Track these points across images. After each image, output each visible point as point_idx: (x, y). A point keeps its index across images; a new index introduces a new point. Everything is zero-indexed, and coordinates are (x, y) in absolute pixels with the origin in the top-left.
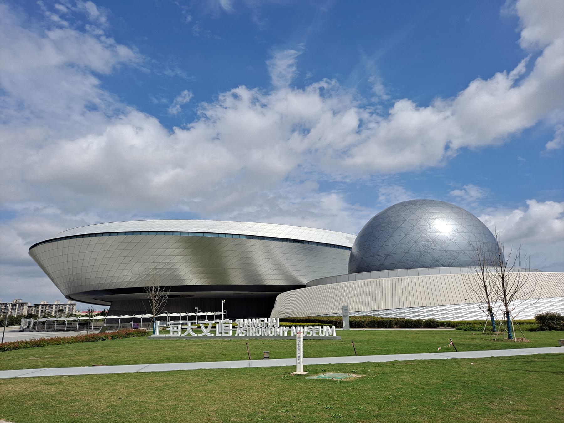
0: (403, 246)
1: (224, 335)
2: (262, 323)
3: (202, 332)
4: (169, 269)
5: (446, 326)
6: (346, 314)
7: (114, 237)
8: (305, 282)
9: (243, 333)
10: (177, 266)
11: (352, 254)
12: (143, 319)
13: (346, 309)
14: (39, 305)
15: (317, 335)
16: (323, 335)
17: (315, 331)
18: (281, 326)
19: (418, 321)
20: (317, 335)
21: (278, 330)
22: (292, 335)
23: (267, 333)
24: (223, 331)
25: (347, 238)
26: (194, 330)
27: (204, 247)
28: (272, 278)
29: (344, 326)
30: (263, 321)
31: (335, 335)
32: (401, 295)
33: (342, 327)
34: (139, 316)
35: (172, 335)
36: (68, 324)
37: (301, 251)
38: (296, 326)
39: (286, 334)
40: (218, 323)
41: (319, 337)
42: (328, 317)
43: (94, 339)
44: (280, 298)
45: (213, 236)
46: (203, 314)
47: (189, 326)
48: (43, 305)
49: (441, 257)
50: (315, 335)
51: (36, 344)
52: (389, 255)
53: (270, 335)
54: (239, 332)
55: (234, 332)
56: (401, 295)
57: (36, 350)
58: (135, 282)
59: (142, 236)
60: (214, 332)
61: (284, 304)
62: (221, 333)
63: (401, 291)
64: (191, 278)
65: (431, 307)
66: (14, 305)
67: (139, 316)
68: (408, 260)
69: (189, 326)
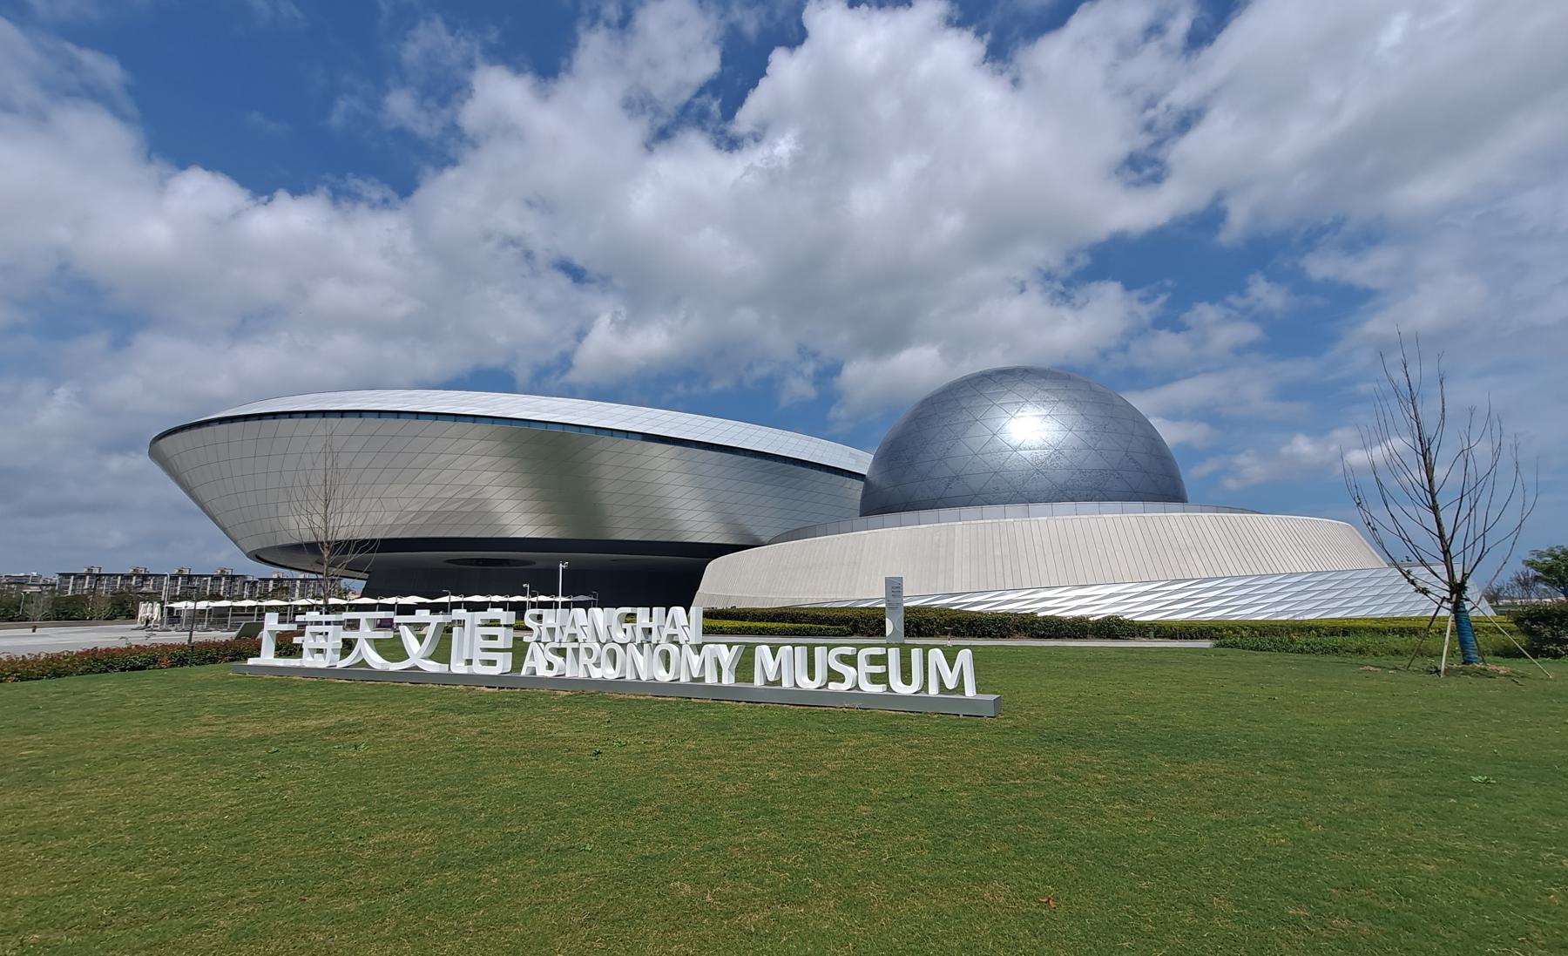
0: (987, 457)
2: (628, 626)
3: (404, 656)
4: (469, 501)
8: (764, 539)
9: (550, 666)
10: (487, 495)
12: (235, 609)
13: (894, 586)
15: (879, 689)
17: (865, 668)
19: (1081, 619)
20: (879, 689)
21: (696, 660)
22: (758, 682)
23: (647, 668)
24: (478, 656)
26: (379, 646)
27: (551, 454)
28: (698, 526)
29: (889, 630)
30: (631, 618)
31: (970, 692)
32: (998, 562)
35: (308, 661)
39: (728, 680)
40: (461, 623)
44: (715, 570)
45: (568, 431)
47: (365, 632)
50: (868, 688)
51: (99, 663)
52: (957, 477)
53: (663, 676)
54: (539, 663)
56: (998, 562)
57: (51, 686)
59: (402, 421)
60: (442, 652)
61: (722, 582)
62: (469, 662)
63: (998, 553)
64: (517, 518)
66: (216, 578)
69: (365, 632)
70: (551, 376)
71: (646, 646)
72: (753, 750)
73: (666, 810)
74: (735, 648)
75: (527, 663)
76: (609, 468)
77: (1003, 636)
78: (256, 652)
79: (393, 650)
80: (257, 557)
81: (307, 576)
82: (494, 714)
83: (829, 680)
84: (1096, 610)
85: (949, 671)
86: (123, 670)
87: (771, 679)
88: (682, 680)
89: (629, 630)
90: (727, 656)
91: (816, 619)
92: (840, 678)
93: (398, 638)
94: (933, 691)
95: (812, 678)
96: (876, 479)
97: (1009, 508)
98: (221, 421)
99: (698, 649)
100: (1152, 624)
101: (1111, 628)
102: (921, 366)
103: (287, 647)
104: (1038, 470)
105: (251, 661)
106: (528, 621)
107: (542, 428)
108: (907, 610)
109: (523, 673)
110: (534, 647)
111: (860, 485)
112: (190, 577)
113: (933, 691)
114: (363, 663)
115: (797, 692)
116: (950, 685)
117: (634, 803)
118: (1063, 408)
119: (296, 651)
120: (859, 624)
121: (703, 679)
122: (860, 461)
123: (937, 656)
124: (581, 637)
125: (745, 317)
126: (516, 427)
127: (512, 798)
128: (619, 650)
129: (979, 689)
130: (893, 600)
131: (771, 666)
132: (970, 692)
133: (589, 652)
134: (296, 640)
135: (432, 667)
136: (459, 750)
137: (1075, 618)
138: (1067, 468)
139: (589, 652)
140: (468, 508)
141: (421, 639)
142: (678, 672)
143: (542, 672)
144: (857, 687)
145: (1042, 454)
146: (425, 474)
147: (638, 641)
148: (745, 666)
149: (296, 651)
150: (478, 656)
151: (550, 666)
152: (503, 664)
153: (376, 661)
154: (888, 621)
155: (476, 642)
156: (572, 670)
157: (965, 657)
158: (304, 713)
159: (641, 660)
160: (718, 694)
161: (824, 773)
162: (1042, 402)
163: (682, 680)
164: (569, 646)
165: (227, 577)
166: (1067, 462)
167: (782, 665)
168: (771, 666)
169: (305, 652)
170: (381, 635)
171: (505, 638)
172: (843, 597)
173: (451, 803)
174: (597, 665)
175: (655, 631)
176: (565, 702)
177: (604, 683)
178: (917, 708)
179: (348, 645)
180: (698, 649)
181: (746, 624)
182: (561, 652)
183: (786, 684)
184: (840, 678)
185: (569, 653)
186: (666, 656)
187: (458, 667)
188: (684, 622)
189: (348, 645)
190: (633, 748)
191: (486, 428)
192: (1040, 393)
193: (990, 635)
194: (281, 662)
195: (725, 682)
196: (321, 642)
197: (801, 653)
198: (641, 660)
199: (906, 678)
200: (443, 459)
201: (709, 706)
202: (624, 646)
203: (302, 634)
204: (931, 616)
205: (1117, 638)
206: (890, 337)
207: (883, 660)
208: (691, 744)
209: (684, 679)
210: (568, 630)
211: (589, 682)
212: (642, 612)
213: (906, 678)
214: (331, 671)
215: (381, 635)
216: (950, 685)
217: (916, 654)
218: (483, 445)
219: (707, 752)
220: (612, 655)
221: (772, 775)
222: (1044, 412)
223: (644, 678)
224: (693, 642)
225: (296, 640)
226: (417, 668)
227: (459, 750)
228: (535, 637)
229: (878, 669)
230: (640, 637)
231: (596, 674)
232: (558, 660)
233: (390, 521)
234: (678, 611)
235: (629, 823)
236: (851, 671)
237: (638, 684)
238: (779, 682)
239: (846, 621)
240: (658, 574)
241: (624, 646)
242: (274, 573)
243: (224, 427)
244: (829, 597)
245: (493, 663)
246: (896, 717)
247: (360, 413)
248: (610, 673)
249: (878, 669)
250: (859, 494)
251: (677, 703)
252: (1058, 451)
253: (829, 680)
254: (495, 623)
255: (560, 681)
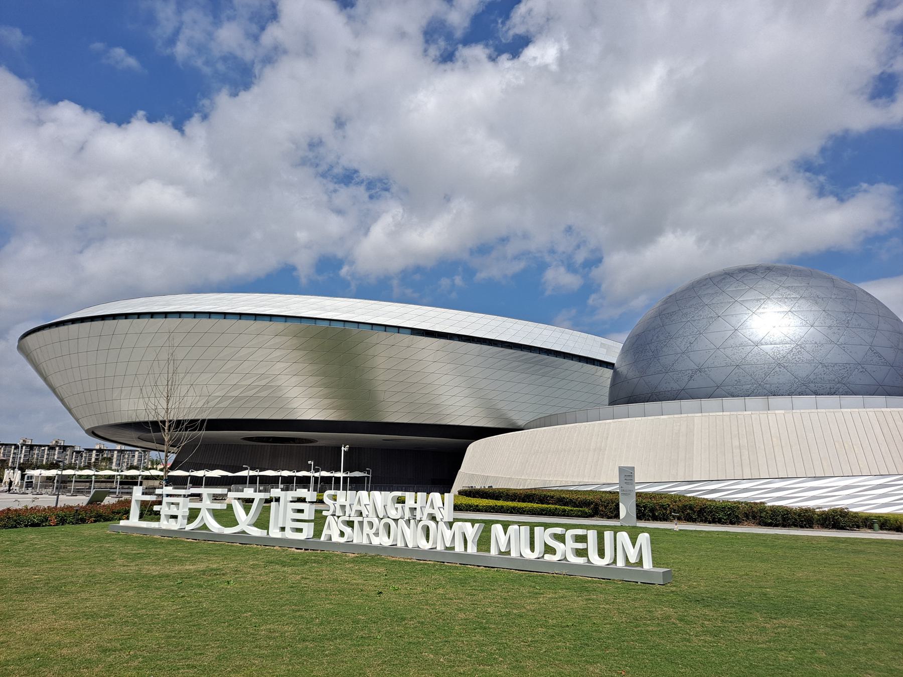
0: (729, 352)
1: (290, 535)
3: (235, 523)
4: (265, 387)
5: (876, 526)
6: (629, 487)
7: (160, 321)
8: (521, 423)
9: (342, 534)
11: (616, 374)
13: (627, 474)
14: (90, 450)
16: (602, 563)
17: (571, 544)
18: (456, 520)
20: (581, 561)
21: (448, 534)
22: (494, 552)
23: (413, 538)
24: (290, 525)
25: (603, 345)
27: (334, 347)
28: (461, 412)
29: (622, 514)
30: (401, 501)
31: (647, 565)
33: (617, 516)
34: (200, 473)
35: (165, 524)
36: (96, 482)
37: (516, 364)
38: (506, 526)
39: (472, 549)
40: (278, 500)
41: (590, 567)
42: (577, 492)
43: (76, 517)
44: (475, 450)
45: (348, 327)
46: (324, 474)
47: (206, 504)
48: (97, 451)
49: (812, 377)
52: (700, 370)
53: (425, 545)
54: (333, 531)
55: (318, 533)
58: (202, 410)
60: (262, 522)
61: (480, 465)
62: (283, 529)
64: (304, 401)
65: (816, 478)
66: (52, 448)
67: (200, 473)
68: (739, 381)
69: (206, 504)
70: (330, 276)
71: (412, 521)
72: (481, 596)
73: (422, 623)
74: (477, 525)
75: (325, 532)
76: (383, 358)
77: (732, 523)
78: (126, 514)
79: (226, 517)
80: (93, 433)
81: (123, 447)
82: (307, 567)
83: (546, 552)
84: (822, 503)
85: (630, 549)
86: (26, 526)
87: (503, 550)
88: (438, 548)
89: (400, 509)
90: (472, 532)
91: (561, 501)
92: (552, 551)
93: (230, 507)
94: (620, 563)
95: (532, 549)
96: (623, 369)
97: (750, 401)
98: (74, 321)
99: (450, 525)
100: (878, 517)
101: (836, 519)
102: (676, 252)
103: (148, 512)
104: (780, 363)
105: (123, 523)
106: (326, 499)
107: (326, 324)
108: (639, 495)
109: (323, 538)
110: (330, 519)
111: (609, 373)
112: (32, 447)
113: (620, 563)
114: (205, 527)
115: (521, 559)
116: (633, 560)
117: (404, 619)
118: (805, 305)
119: (156, 516)
120: (597, 507)
121: (453, 548)
122: (609, 349)
123: (623, 536)
124: (365, 513)
125: (505, 217)
126: (305, 324)
127: (332, 613)
128: (392, 524)
129: (656, 563)
130: (626, 487)
131: (503, 540)
132: (647, 565)
133: (371, 524)
134: (156, 508)
135: (255, 532)
136: (292, 587)
137: (801, 509)
138: (809, 362)
139: (371, 524)
140: (264, 394)
141: (247, 510)
142: (435, 542)
143: (336, 538)
144: (565, 559)
145: (784, 349)
146: (230, 364)
147: (406, 518)
148: (484, 541)
149: (156, 516)
150: (290, 525)
151: (342, 534)
152: (308, 530)
153: (214, 526)
154: (621, 506)
155: (288, 516)
156: (357, 537)
157: (644, 538)
158: (181, 561)
159: (408, 532)
160: (465, 560)
161: (524, 610)
162: (783, 299)
163: (438, 548)
164: (356, 520)
165: (60, 447)
166: (809, 357)
167: (513, 540)
168: (503, 540)
169: (162, 517)
170: (218, 506)
171: (309, 511)
172: (590, 481)
173: (298, 613)
174: (377, 534)
175: (418, 510)
176: (354, 561)
177: (381, 548)
178: (606, 579)
179: (193, 515)
180: (450, 525)
181: (500, 503)
182: (350, 524)
183: (514, 554)
184: (552, 551)
185: (356, 525)
186: (427, 530)
187: (275, 533)
188: (440, 503)
189: (193, 515)
190: (403, 592)
191: (280, 326)
192: (782, 291)
193: (719, 521)
194: (144, 524)
195: (469, 551)
196: (174, 511)
197: (525, 530)
198: (408, 532)
199: (601, 554)
200: (244, 352)
201: (457, 568)
202: (396, 520)
203: (160, 503)
204: (665, 502)
205: (842, 528)
206: (645, 231)
207: (582, 539)
208: (441, 591)
209: (440, 548)
210: (356, 507)
211: (370, 547)
212: (409, 496)
213: (601, 554)
214: (181, 532)
215: (218, 506)
216: (633, 560)
217: (608, 535)
218: (278, 340)
219: (451, 595)
220: (388, 528)
221: (489, 610)
222: (786, 308)
223: (410, 546)
224: (446, 520)
225: (156, 508)
226: (244, 532)
227: (292, 587)
228: (331, 512)
229: (580, 546)
230: (407, 515)
231: (376, 541)
232: (347, 530)
233: (200, 404)
234: (436, 496)
235: (400, 628)
236: (559, 545)
237: (406, 550)
238: (508, 553)
239: (586, 503)
240: (424, 458)
241: (396, 520)
242: (97, 444)
243: (76, 326)
244: (577, 480)
245: (300, 530)
246: (590, 581)
247: (180, 314)
248: (386, 542)
249: (580, 546)
250: (608, 383)
251: (434, 565)
252: (800, 346)
253: (546, 552)
254: (302, 500)
255: (349, 544)
